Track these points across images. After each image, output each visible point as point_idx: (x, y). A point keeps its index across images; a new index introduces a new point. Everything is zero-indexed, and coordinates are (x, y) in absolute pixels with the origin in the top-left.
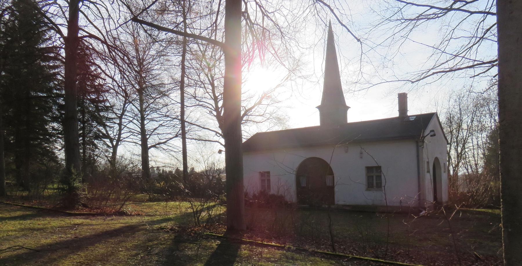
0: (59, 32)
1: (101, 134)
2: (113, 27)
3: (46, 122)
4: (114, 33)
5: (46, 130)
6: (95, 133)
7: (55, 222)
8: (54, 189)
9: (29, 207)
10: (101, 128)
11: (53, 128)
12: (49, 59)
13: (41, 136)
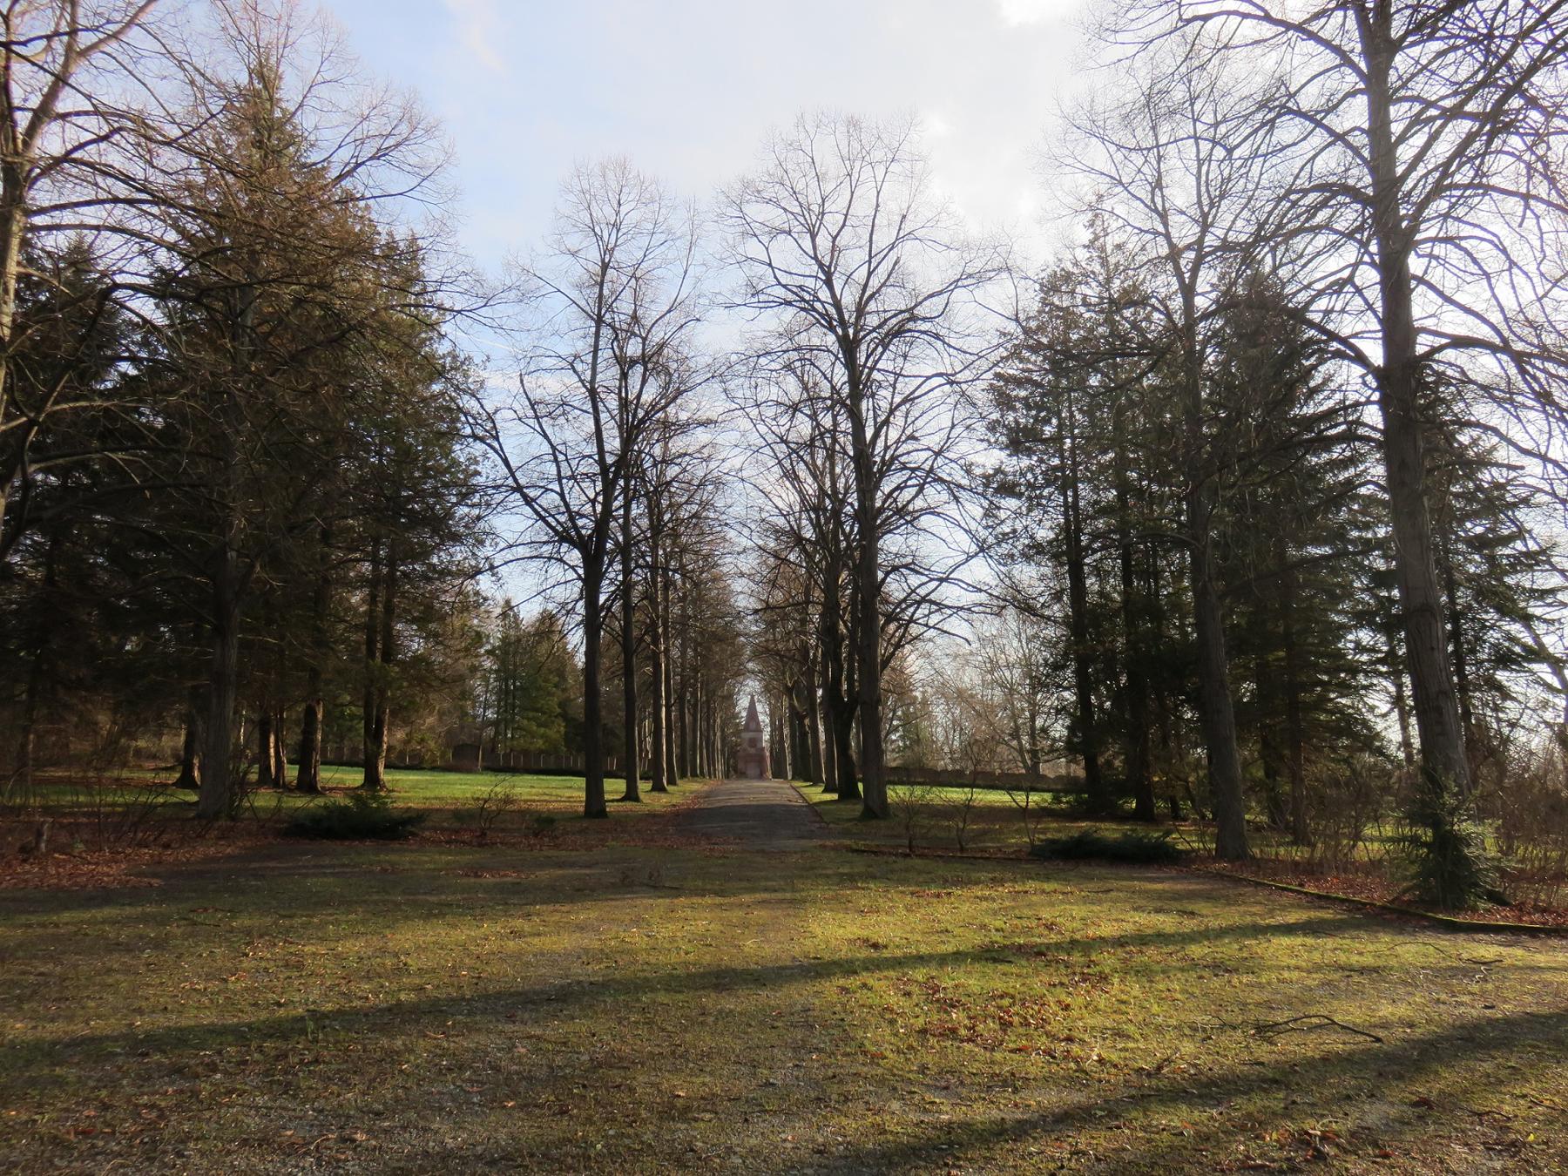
0: (1360, 358)
1: (1517, 649)
2: (1527, 295)
3: (1340, 631)
4: (1534, 312)
5: (1340, 655)
6: (1496, 647)
7: (1413, 950)
8: (1383, 840)
9: (1319, 897)
10: (1516, 628)
11: (1359, 648)
12: (1327, 443)
13: (1326, 673)
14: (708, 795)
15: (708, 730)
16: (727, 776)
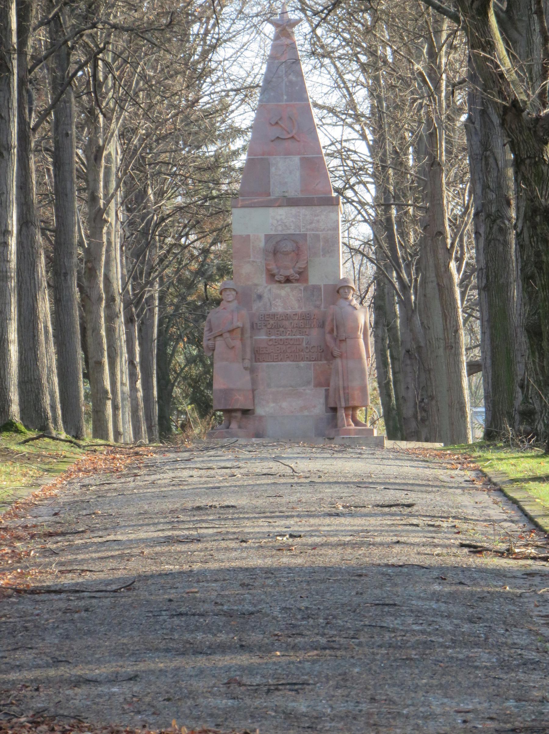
14: (61, 528)
15: (61, 198)
16: (162, 426)
